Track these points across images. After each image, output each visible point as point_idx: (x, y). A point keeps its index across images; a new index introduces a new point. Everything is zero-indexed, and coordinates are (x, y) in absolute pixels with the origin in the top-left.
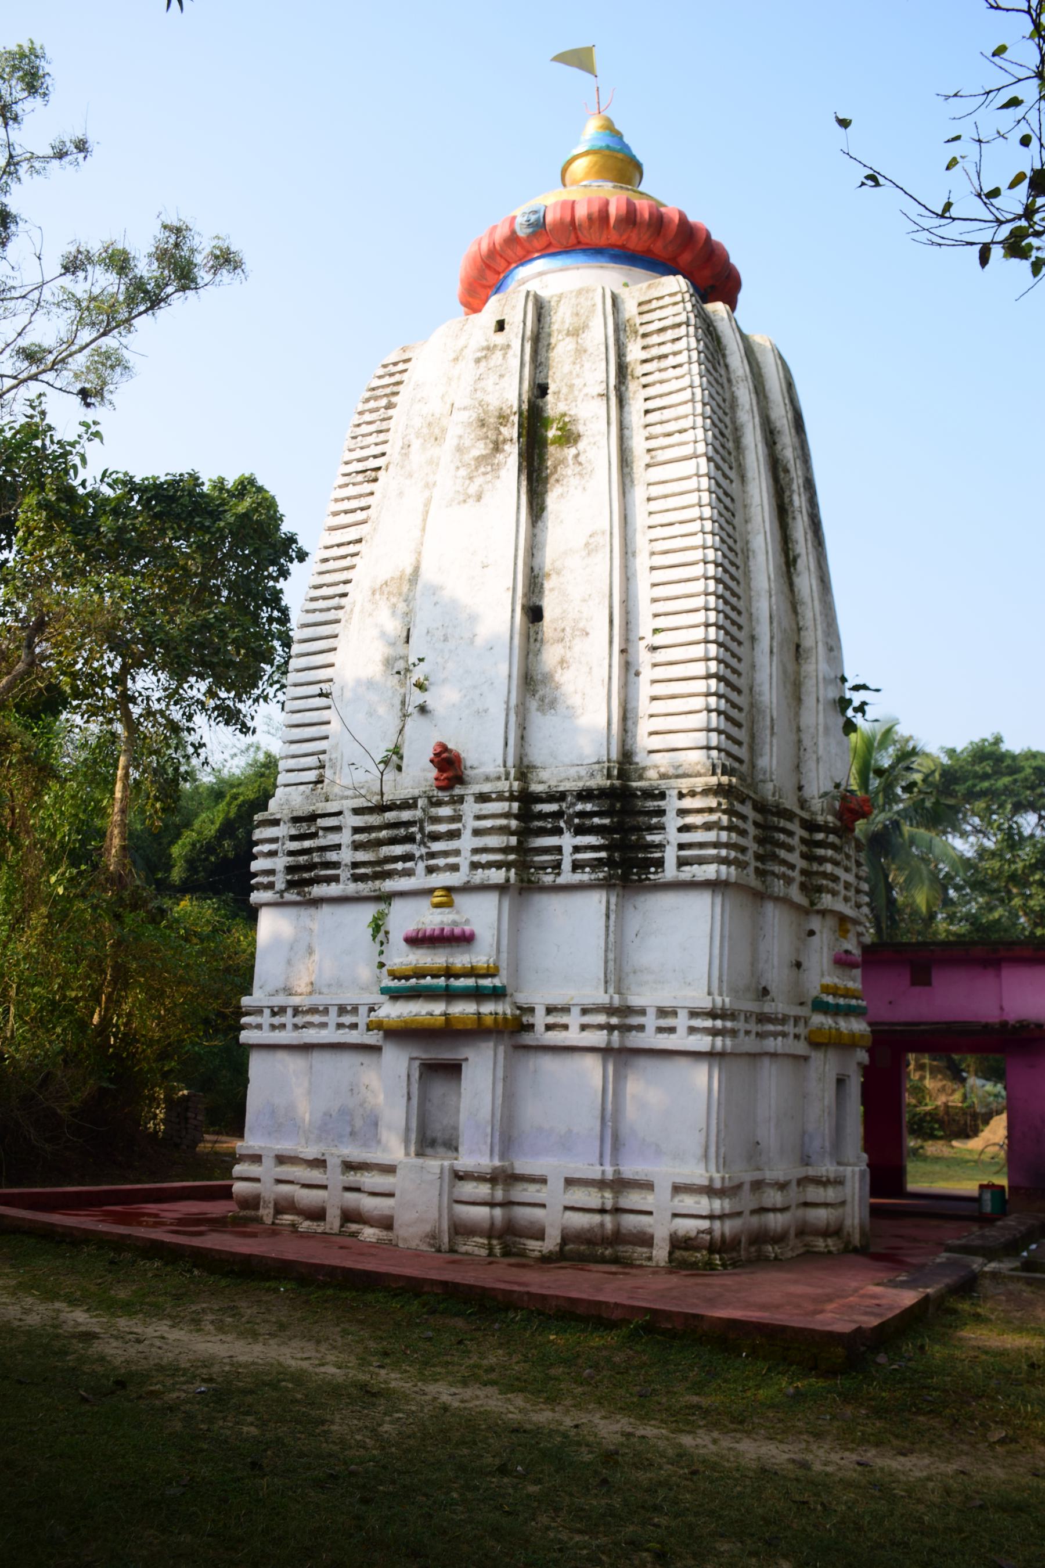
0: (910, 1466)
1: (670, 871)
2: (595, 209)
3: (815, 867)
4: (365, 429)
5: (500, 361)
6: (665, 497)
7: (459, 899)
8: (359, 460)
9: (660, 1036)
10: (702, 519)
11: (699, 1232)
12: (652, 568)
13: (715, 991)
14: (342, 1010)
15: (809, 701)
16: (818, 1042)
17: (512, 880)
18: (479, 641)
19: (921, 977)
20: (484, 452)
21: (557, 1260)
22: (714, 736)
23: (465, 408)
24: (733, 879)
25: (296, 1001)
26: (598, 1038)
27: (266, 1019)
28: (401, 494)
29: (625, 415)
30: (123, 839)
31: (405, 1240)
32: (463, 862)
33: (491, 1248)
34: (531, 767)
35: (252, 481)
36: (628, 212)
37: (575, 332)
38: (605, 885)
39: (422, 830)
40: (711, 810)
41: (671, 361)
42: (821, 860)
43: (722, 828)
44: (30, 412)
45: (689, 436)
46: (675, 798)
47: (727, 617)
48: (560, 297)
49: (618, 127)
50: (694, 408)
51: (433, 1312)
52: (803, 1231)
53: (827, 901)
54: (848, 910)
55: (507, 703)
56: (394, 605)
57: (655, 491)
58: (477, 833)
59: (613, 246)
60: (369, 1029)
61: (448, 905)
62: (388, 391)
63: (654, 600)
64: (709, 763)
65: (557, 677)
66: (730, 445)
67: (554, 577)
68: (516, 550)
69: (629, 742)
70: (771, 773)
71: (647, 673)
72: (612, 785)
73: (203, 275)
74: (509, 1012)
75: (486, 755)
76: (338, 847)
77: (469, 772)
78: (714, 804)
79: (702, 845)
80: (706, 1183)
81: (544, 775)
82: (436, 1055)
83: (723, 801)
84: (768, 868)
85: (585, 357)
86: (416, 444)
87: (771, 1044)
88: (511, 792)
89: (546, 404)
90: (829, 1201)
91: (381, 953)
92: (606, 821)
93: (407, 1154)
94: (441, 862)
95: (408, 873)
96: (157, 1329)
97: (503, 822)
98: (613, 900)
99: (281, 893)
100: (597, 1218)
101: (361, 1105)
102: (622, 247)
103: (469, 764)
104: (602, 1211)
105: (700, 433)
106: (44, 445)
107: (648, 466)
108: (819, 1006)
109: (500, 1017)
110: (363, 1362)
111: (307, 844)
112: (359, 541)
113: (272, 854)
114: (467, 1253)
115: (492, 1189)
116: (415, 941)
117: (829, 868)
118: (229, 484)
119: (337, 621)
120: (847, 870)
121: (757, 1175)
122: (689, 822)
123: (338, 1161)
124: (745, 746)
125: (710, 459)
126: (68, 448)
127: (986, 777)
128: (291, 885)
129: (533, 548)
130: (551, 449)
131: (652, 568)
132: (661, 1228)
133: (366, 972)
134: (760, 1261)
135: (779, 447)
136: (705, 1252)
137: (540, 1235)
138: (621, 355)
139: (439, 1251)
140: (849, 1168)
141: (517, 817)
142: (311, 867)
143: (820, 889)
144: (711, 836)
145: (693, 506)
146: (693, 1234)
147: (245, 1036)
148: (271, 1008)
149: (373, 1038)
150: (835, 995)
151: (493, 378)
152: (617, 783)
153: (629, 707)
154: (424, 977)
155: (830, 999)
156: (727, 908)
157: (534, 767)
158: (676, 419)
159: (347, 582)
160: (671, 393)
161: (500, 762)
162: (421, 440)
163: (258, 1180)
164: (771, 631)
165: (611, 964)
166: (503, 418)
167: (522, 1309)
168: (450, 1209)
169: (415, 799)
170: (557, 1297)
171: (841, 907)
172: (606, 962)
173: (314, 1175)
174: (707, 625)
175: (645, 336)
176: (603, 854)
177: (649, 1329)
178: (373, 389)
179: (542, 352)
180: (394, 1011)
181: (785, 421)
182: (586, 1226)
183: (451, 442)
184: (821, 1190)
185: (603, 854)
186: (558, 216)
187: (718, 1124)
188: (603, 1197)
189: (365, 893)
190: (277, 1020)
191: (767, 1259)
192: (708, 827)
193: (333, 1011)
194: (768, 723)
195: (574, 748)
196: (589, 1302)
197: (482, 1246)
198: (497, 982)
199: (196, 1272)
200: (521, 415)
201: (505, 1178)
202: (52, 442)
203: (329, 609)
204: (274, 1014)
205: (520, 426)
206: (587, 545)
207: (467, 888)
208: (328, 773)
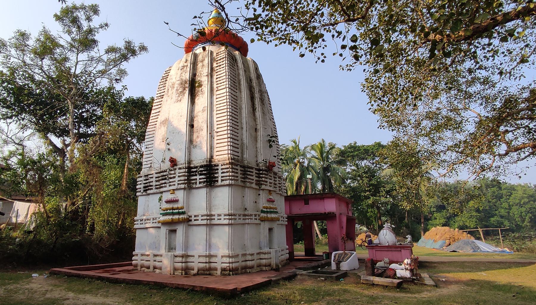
1: (220, 183)
4: (161, 86)
7: (175, 192)
15: (259, 141)
16: (263, 220)
19: (307, 203)
26: (205, 222)
30: (126, 182)
32: (176, 183)
37: (202, 61)
38: (206, 186)
40: (228, 168)
41: (222, 66)
45: (225, 83)
47: (233, 124)
52: (259, 266)
54: (271, 189)
57: (218, 96)
58: (179, 177)
63: (217, 121)
71: (216, 138)
75: (181, 158)
76: (152, 182)
79: (226, 176)
82: (171, 226)
86: (170, 89)
87: (247, 221)
94: (172, 184)
95: (166, 187)
100: (205, 264)
104: (206, 263)
108: (262, 212)
111: (147, 181)
113: (141, 184)
116: (167, 202)
117: (264, 179)
121: (245, 252)
125: (229, 88)
127: (352, 152)
128: (144, 191)
132: (219, 266)
134: (246, 273)
138: (212, 65)
142: (148, 186)
143: (262, 184)
144: (228, 174)
147: (135, 226)
149: (160, 225)
151: (184, 73)
155: (265, 210)
166: (186, 82)
177: (192, 290)
180: (163, 218)
183: (175, 88)
190: (141, 222)
192: (227, 172)
195: (200, 157)
198: (183, 210)
207: (177, 189)
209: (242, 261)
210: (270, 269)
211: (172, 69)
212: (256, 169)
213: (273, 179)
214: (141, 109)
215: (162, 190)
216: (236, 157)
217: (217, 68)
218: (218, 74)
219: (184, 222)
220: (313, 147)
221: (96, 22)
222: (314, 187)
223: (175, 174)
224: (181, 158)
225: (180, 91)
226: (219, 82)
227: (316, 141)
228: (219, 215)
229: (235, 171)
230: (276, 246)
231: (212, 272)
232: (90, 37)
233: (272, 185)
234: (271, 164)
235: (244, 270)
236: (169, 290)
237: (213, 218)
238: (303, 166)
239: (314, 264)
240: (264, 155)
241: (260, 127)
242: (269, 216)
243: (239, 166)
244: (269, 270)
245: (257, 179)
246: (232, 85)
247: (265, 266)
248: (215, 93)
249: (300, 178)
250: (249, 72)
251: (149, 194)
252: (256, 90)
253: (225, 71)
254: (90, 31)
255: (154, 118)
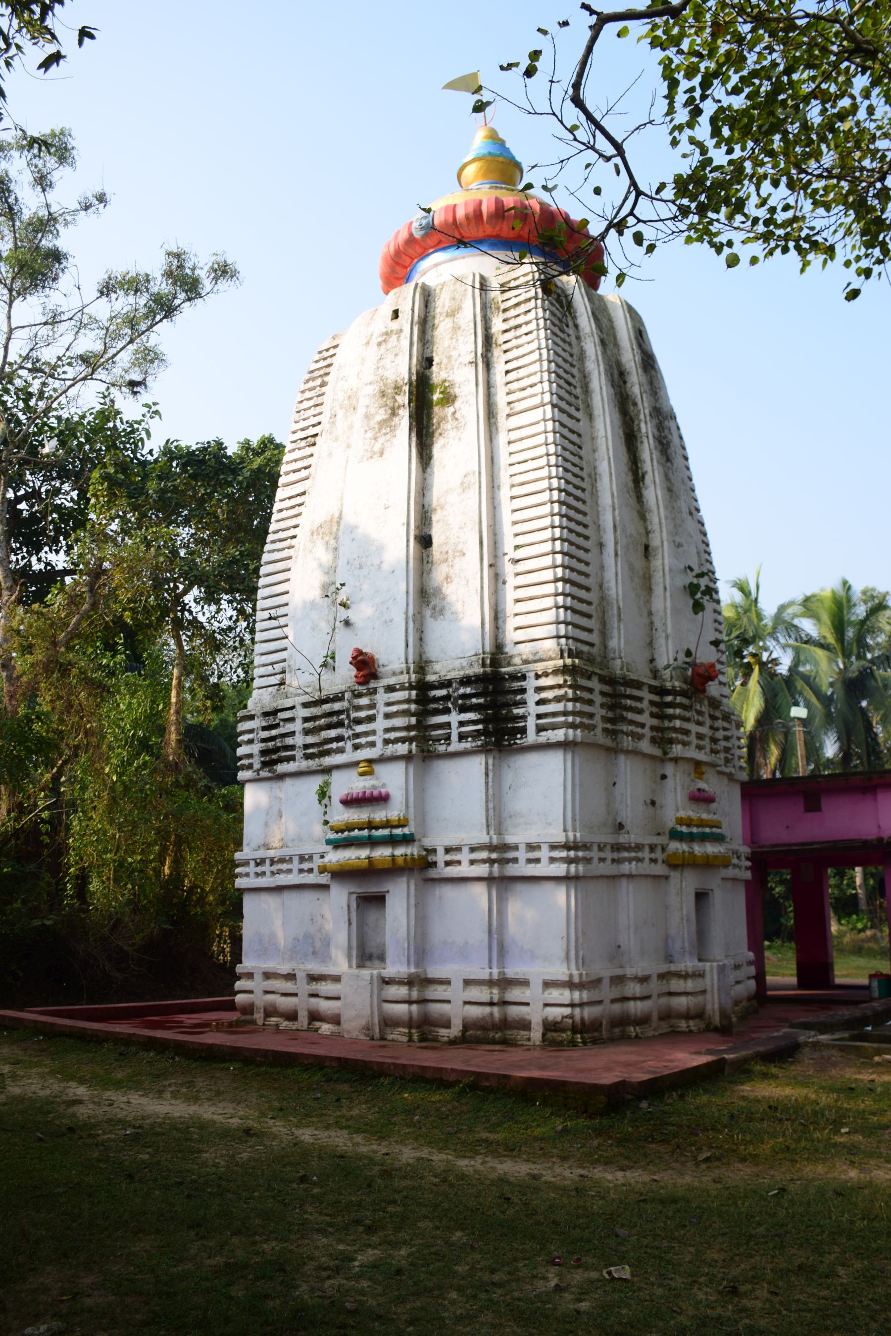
0: (612, 1177)
1: (531, 737)
2: (471, 209)
3: (666, 724)
4: (306, 404)
5: (395, 343)
6: (522, 439)
7: (378, 769)
8: (303, 430)
9: (530, 866)
10: (548, 455)
11: (563, 1017)
12: (513, 498)
13: (569, 827)
14: (302, 859)
15: (658, 590)
16: (677, 864)
17: (414, 751)
18: (385, 567)
19: (813, 805)
20: (384, 417)
21: (461, 1043)
22: (562, 627)
23: (370, 383)
24: (579, 740)
25: (271, 853)
26: (482, 870)
27: (252, 869)
28: (330, 455)
29: (492, 376)
30: (179, 734)
31: (348, 1032)
32: (378, 739)
33: (410, 1036)
34: (429, 662)
35: (271, 440)
36: (497, 209)
37: (452, 314)
38: (483, 750)
39: (348, 716)
40: (559, 686)
42: (672, 718)
43: (569, 700)
44: (102, 401)
45: (538, 389)
46: (533, 679)
47: (571, 531)
48: (443, 285)
49: (501, 136)
50: (541, 365)
51: (329, 1080)
52: (667, 1015)
53: (677, 750)
54: (701, 756)
55: (406, 613)
56: (327, 543)
57: (514, 435)
58: (387, 716)
59: (490, 237)
60: (321, 873)
61: (370, 773)
62: (322, 372)
63: (515, 523)
64: (557, 649)
65: (444, 590)
66: (578, 391)
67: (439, 511)
68: (409, 492)
69: (501, 636)
70: (620, 651)
72: (485, 672)
73: (207, 284)
74: (415, 853)
75: (393, 656)
76: (293, 733)
77: (381, 669)
78: (561, 682)
79: (554, 714)
80: (567, 979)
81: (437, 667)
82: (367, 887)
83: (568, 678)
84: (618, 728)
85: (459, 333)
87: (626, 868)
88: (410, 683)
89: (432, 373)
90: (688, 990)
91: (326, 813)
92: (481, 701)
93: (350, 966)
94: (363, 740)
95: (341, 751)
96: (135, 1098)
97: (405, 706)
98: (491, 762)
99: (258, 771)
100: (487, 1010)
101: (319, 931)
102: (497, 236)
103: (381, 663)
104: (491, 1004)
105: (546, 385)
106: (115, 426)
107: (509, 416)
108: (675, 835)
109: (409, 857)
110: (263, 1115)
111: (274, 732)
112: (304, 493)
113: (250, 742)
114: (393, 1040)
115: (410, 990)
116: (349, 802)
117: (678, 723)
118: (255, 443)
119: (290, 558)
120: (699, 723)
121: (619, 972)
122: (543, 696)
123: (304, 975)
124: (596, 633)
125: (554, 406)
126: (136, 426)
128: (264, 764)
129: (423, 489)
130: (436, 409)
131: (513, 498)
132: (536, 1015)
133: (318, 830)
134: (623, 1039)
135: (629, 385)
136: (569, 1033)
137: (447, 1025)
138: (487, 328)
139: (372, 1039)
140: (708, 964)
141: (416, 702)
143: (671, 741)
144: (559, 707)
145: (540, 445)
146: (559, 1019)
148: (255, 860)
149: (324, 879)
150: (688, 825)
151: (390, 357)
152: (488, 669)
153: (500, 609)
154: (353, 830)
155: (684, 829)
156: (577, 762)
157: (431, 662)
158: (528, 376)
159: (296, 527)
160: (524, 355)
161: (403, 660)
162: (344, 410)
163: (251, 992)
164: (615, 538)
165: (491, 812)
166: (397, 389)
167: (390, 1075)
168: (380, 1008)
169: (343, 693)
170: (413, 1066)
171: (692, 753)
172: (487, 810)
173: (288, 986)
174: (554, 540)
175: (505, 310)
176: (480, 727)
177: (474, 1087)
178: (312, 372)
179: (429, 332)
180: (335, 857)
181: (633, 364)
182: (480, 1016)
183: (361, 411)
184: (682, 982)
185: (480, 727)
186: (443, 218)
187: (576, 932)
188: (491, 993)
189: (314, 768)
190: (260, 869)
191: (629, 1037)
192: (558, 699)
193: (296, 860)
194: (615, 612)
195: (457, 647)
196: (434, 1068)
197: (403, 1034)
198: (406, 831)
199: (177, 1059)
200: (411, 384)
201: (419, 981)
202: (122, 422)
203: (283, 549)
204: (257, 864)
205: (410, 393)
206: (462, 483)
207: (383, 760)
208: (288, 677)
209: (613, 1001)
210: (702, 1026)
211: (343, 342)
212: (653, 690)
213: (708, 722)
214: (231, 495)
215: (328, 761)
216: (585, 648)
217: (507, 336)
218: (510, 355)
219: (411, 869)
220: (808, 605)
221: (68, 187)
222: (813, 750)
223: (372, 706)
224: (393, 656)
225: (379, 418)
226: (515, 386)
227: (824, 584)
228: (531, 847)
229: (586, 695)
230: (717, 950)
231: (511, 1034)
232: (47, 243)
233: (706, 742)
234: (701, 670)
235: (614, 1030)
236: (392, 1084)
237: (511, 855)
238: (773, 675)
239: (846, 1013)
240: (675, 640)
241: (660, 538)
242: (698, 849)
243: (595, 679)
244: (700, 1032)
245: (655, 722)
246: (563, 393)
247: (687, 1016)
248: (503, 423)
249: (764, 720)
250: (616, 345)
251: (282, 777)
252: (644, 408)
253: (535, 345)
254: (45, 224)
255: (285, 514)
